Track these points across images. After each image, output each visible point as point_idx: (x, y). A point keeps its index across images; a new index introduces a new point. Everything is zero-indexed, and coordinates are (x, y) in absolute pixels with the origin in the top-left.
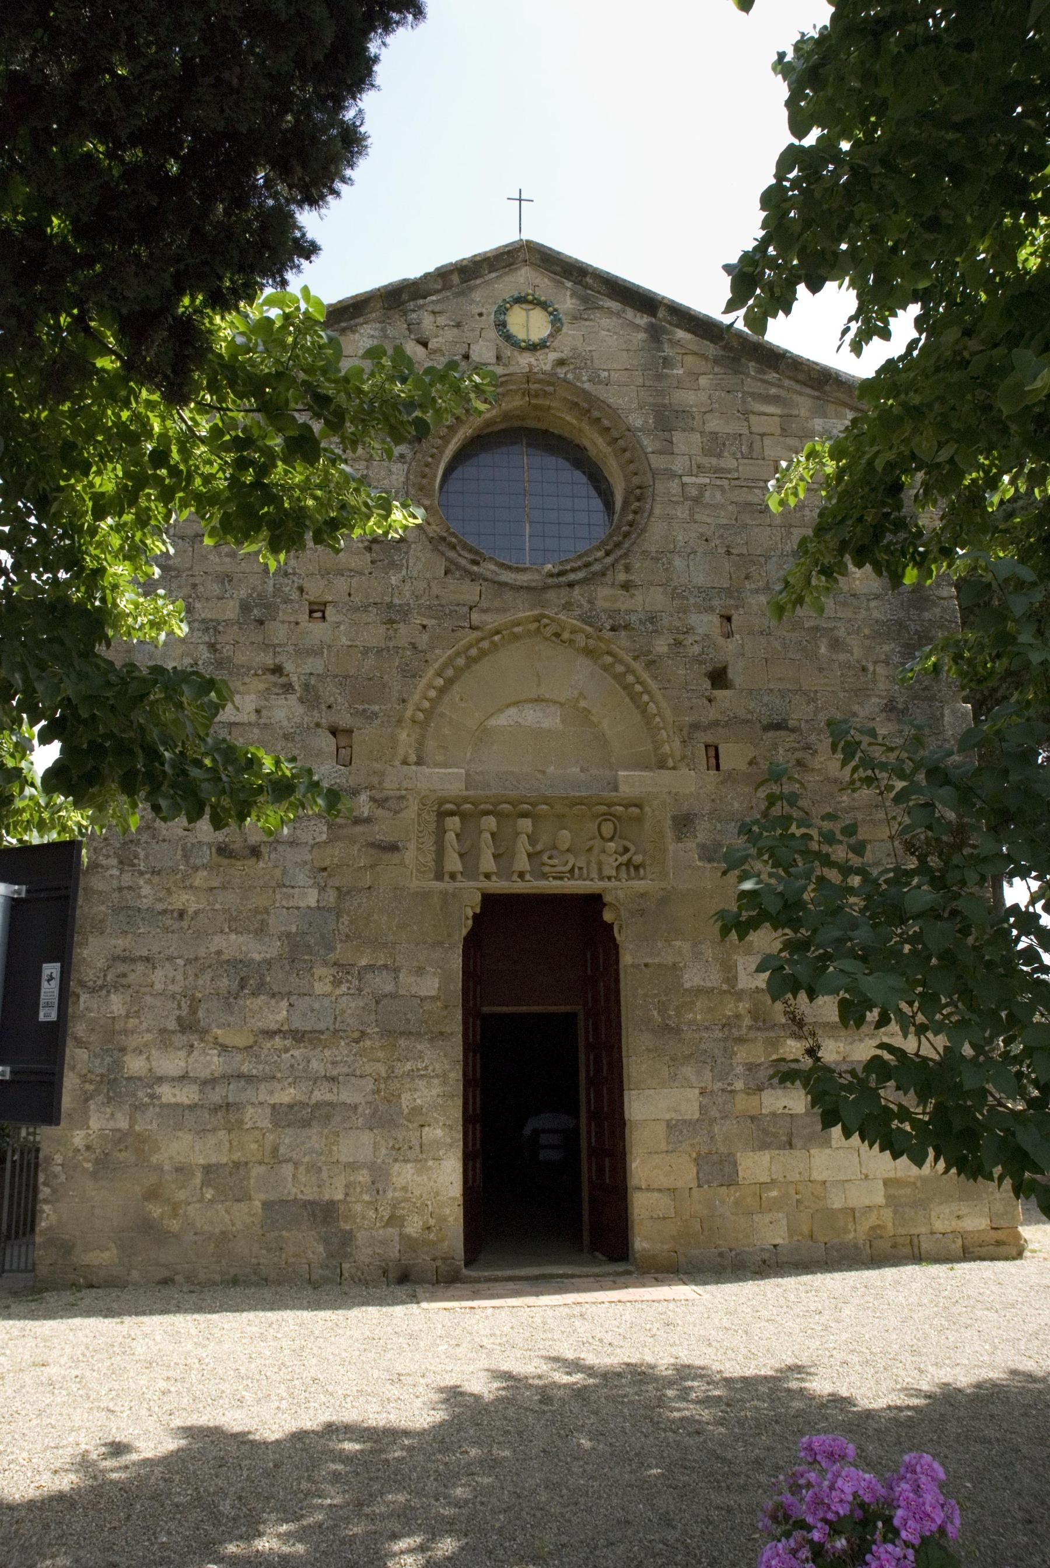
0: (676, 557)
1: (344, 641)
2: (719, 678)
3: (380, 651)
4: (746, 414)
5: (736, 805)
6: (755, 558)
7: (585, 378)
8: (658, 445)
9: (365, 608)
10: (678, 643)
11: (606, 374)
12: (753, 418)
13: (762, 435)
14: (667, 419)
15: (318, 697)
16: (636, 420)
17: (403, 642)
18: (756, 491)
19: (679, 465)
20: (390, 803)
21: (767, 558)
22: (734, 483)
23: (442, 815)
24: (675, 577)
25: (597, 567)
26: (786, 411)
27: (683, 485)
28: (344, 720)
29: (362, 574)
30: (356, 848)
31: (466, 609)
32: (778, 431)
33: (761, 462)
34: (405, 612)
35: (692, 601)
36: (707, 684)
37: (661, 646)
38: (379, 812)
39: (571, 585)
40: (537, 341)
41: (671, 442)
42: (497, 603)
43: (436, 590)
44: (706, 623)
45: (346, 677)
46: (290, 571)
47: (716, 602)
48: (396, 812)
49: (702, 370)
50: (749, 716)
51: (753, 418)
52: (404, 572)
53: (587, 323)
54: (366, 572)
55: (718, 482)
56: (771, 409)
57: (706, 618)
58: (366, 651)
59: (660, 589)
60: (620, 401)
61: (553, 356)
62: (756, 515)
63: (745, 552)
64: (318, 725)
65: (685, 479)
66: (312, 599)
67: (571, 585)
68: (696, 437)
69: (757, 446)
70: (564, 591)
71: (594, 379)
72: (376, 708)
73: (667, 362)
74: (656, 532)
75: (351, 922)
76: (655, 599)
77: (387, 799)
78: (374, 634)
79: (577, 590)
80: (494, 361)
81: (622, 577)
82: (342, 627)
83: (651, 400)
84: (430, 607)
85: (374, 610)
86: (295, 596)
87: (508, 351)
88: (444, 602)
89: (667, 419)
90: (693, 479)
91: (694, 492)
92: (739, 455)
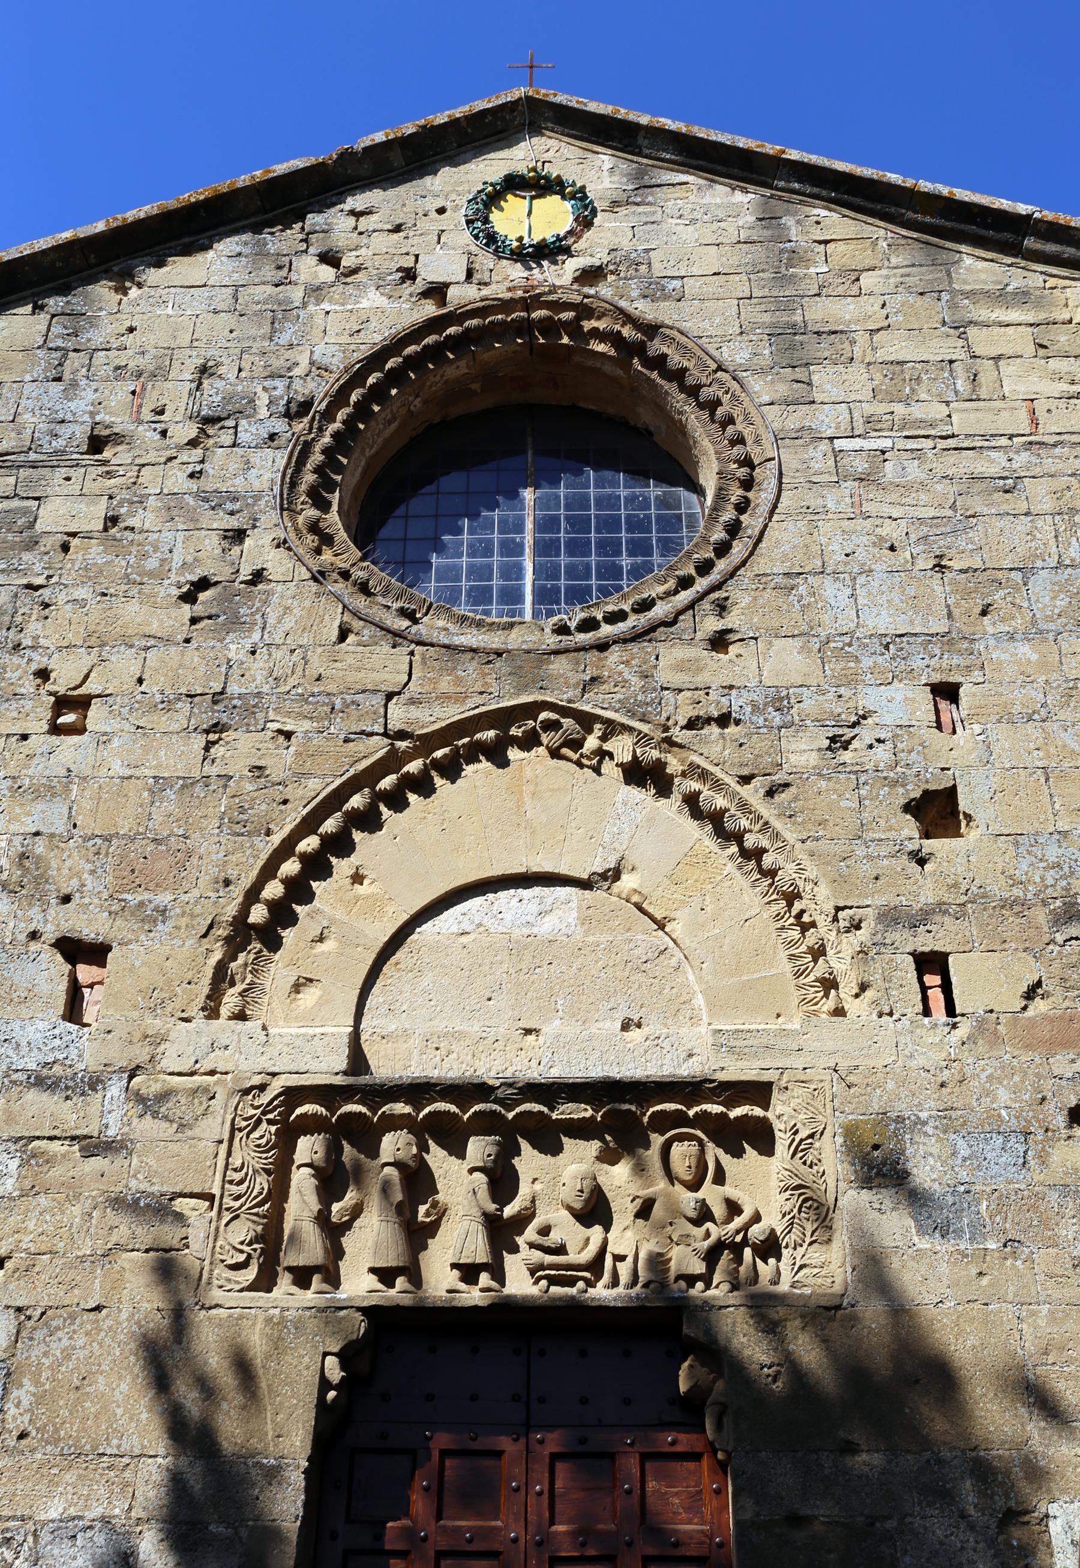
0: (828, 581)
1: (118, 768)
2: (938, 811)
3: (188, 784)
4: (961, 328)
5: (1004, 1096)
6: (999, 575)
7: (635, 294)
8: (782, 390)
9: (168, 705)
10: (838, 743)
11: (676, 283)
12: (972, 332)
13: (997, 359)
14: (795, 346)
15: (41, 880)
16: (736, 354)
17: (239, 767)
18: (993, 454)
19: (827, 419)
20: (177, 1108)
21: (1026, 571)
22: (942, 444)
23: (288, 1135)
24: (826, 618)
25: (660, 610)
26: (1042, 316)
27: (836, 453)
28: (89, 926)
29: (168, 641)
30: (77, 1210)
31: (380, 699)
32: (1031, 349)
33: (999, 404)
34: (250, 708)
35: (867, 662)
36: (909, 827)
37: (802, 752)
38: (147, 1127)
39: (602, 647)
40: (469, 769)
41: (810, 384)
42: (445, 684)
43: (317, 664)
44: (901, 703)
45: (108, 839)
46: (27, 642)
47: (917, 663)
48: (182, 1127)
49: (867, 263)
50: (1017, 892)
51: (972, 332)
52: (256, 636)
53: (641, 209)
54: (180, 638)
55: (911, 444)
56: (1014, 315)
57: (899, 691)
58: (160, 784)
59: (798, 643)
60: (706, 324)
61: (571, 266)
62: (999, 496)
63: (978, 564)
64: (34, 936)
65: (838, 444)
66: (62, 691)
67: (602, 647)
68: (857, 374)
69: (988, 375)
70: (593, 656)
71: (655, 291)
72: (164, 898)
73: (795, 257)
74: (783, 543)
75: (39, 1399)
76: (783, 663)
77: (164, 1096)
78: (180, 755)
79: (614, 655)
80: (462, 277)
81: (712, 624)
82: (116, 742)
83: (767, 318)
84: (303, 699)
85: (184, 706)
86: (28, 686)
87: (485, 260)
88: (332, 688)
89: (795, 346)
90: (857, 443)
91: (861, 465)
92: (951, 396)
